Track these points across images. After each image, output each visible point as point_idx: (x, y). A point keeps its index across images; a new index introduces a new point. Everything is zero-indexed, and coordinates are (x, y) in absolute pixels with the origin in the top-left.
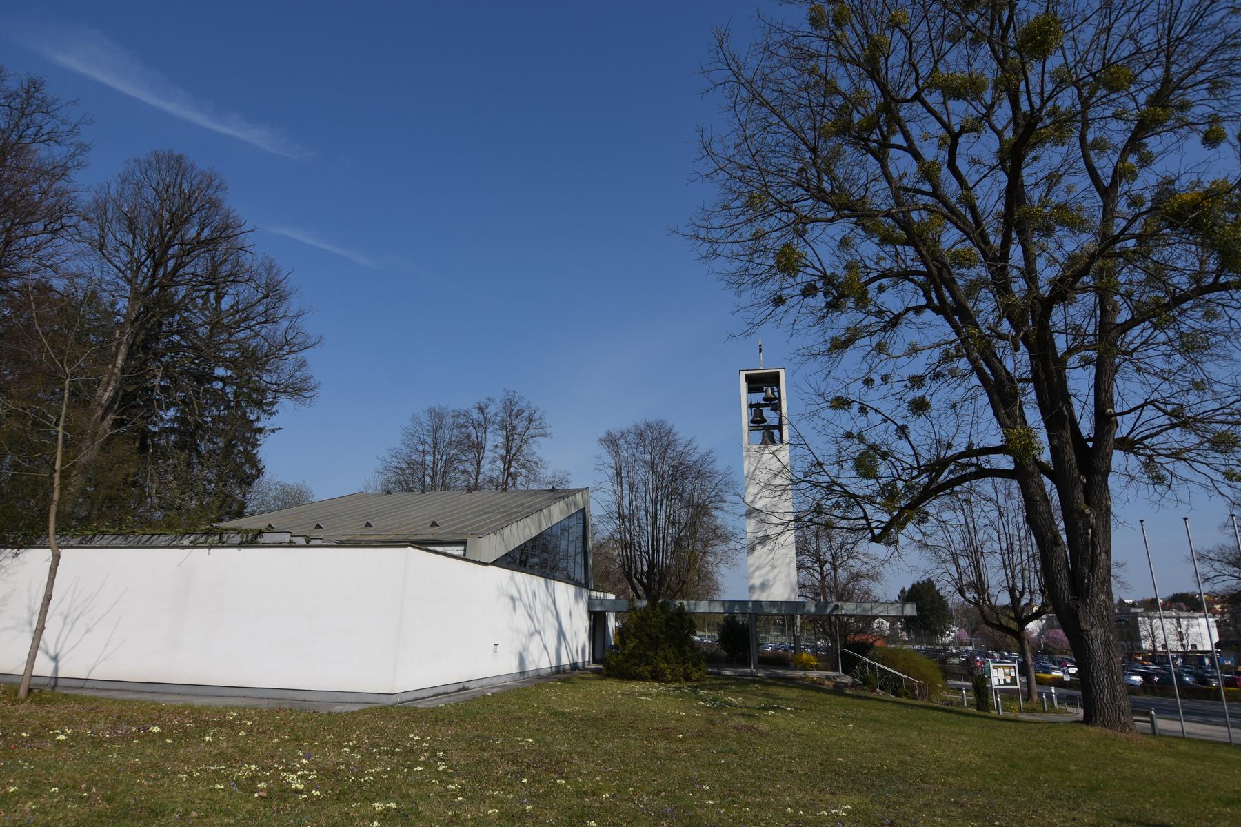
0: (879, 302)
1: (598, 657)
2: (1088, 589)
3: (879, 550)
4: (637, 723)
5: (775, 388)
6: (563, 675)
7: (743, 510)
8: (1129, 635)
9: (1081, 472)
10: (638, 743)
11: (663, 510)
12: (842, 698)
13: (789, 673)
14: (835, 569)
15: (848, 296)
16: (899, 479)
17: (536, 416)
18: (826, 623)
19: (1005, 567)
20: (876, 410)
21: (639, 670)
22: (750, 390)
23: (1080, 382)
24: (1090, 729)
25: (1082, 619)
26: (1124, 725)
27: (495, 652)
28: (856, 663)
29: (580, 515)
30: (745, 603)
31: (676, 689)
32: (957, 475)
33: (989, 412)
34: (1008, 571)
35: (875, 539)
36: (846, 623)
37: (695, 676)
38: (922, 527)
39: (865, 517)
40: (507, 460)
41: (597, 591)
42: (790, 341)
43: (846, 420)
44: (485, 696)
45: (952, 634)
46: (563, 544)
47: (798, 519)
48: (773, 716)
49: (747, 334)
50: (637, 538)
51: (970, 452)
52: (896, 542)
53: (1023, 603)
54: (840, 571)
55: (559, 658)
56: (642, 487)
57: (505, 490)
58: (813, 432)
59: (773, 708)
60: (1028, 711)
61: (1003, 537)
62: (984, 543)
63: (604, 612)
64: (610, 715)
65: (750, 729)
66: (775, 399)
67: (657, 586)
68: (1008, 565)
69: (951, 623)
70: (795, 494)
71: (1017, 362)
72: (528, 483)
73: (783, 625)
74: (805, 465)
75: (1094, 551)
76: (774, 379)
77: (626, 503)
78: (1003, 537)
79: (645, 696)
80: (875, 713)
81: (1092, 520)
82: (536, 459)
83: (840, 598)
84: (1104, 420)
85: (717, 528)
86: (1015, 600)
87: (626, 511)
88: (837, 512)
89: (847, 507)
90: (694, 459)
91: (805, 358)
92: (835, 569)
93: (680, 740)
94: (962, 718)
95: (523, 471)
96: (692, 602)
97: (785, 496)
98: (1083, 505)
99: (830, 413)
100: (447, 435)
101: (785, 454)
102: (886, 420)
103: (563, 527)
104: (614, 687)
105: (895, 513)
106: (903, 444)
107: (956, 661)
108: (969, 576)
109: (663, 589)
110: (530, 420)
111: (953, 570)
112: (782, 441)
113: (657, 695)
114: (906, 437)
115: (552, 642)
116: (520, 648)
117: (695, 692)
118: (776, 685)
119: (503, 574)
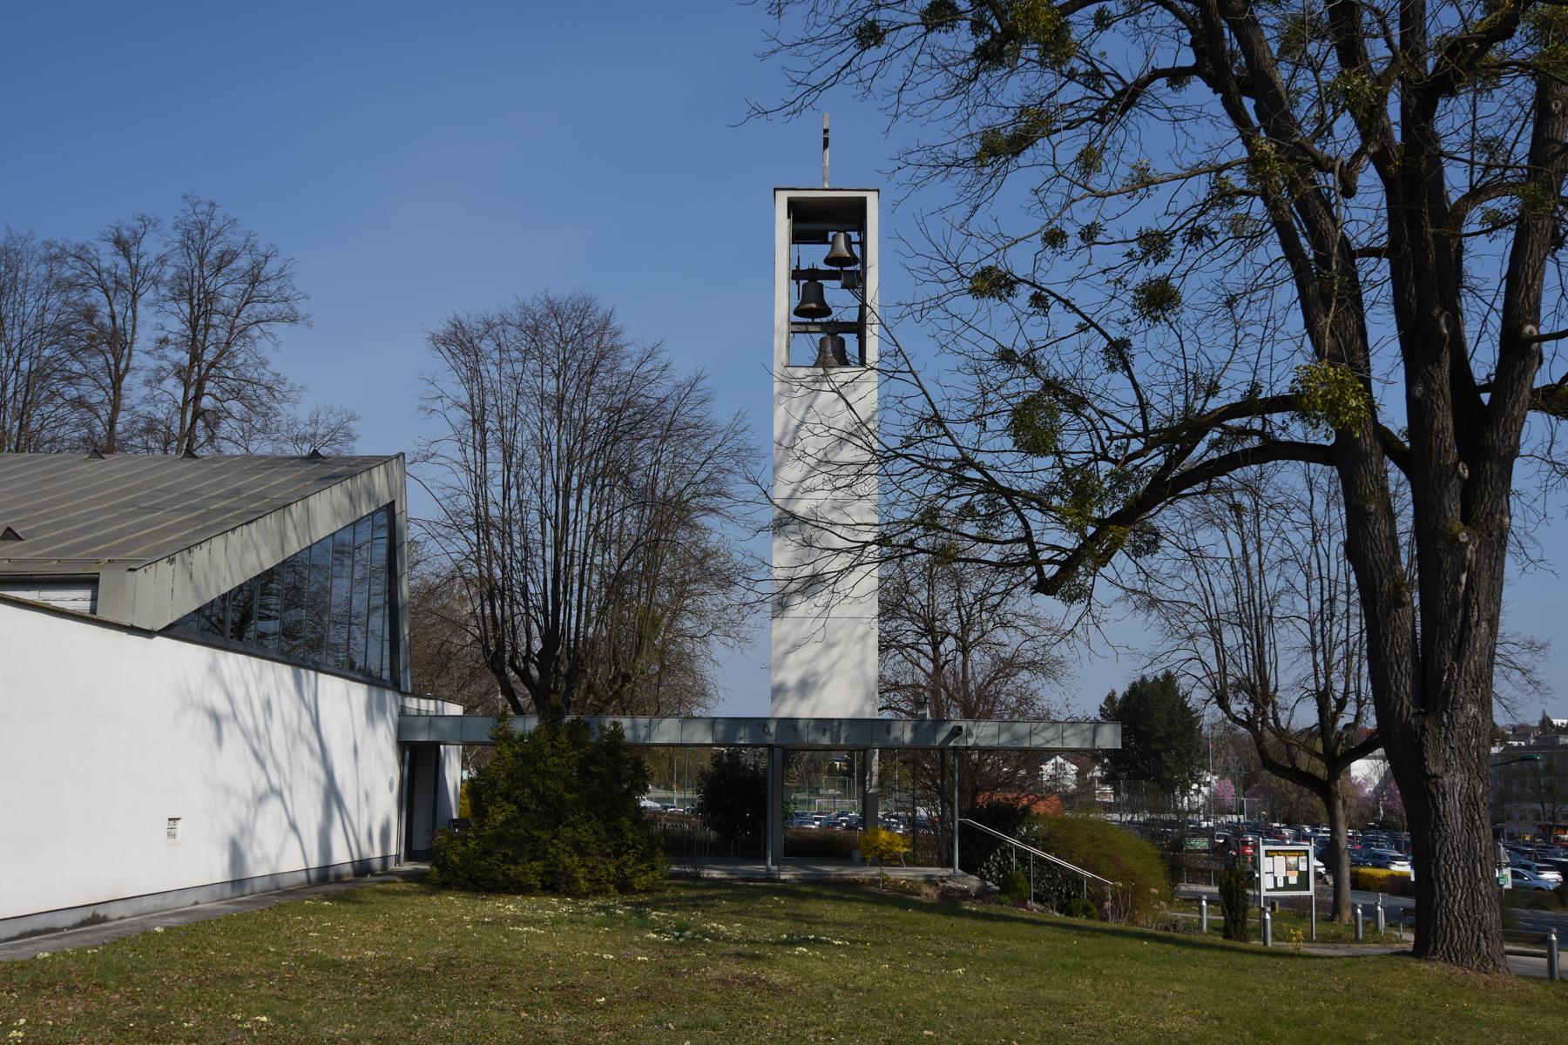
0: (1094, 52)
1: (419, 845)
2: (1447, 693)
3: (1049, 607)
4: (507, 979)
5: (855, 236)
6: (331, 886)
7: (768, 516)
8: (1550, 789)
9: (1462, 457)
10: (508, 1017)
11: (583, 511)
12: (953, 920)
13: (850, 872)
14: (965, 649)
15: (1023, 39)
16: (1105, 458)
17: (271, 268)
18: (938, 767)
19: (1314, 650)
20: (1067, 303)
21: (514, 870)
22: (798, 237)
23: (1486, 260)
24: (1423, 966)
25: (1429, 755)
26: (1485, 959)
27: (171, 835)
28: (991, 849)
29: (382, 519)
30: (760, 723)
31: (599, 908)
32: (1225, 452)
33: (1296, 320)
34: (1320, 657)
35: (1045, 587)
36: (978, 766)
37: (642, 881)
38: (1146, 561)
39: (1028, 538)
40: (194, 378)
41: (420, 696)
42: (892, 131)
43: (1003, 322)
44: (148, 935)
45: (1206, 788)
46: (340, 588)
47: (883, 541)
48: (803, 956)
49: (793, 109)
50: (518, 576)
51: (1252, 404)
52: (1085, 594)
53: (1341, 723)
54: (976, 655)
55: (326, 849)
56: (533, 455)
57: (190, 454)
58: (931, 349)
59: (805, 942)
60: (1325, 939)
61: (1316, 585)
62: (1276, 597)
63: (436, 745)
64: (447, 965)
65: (752, 983)
66: (854, 260)
67: (562, 687)
68: (1319, 645)
69: (1203, 767)
70: (881, 485)
71: (1365, 213)
72: (247, 436)
73: (849, 774)
74: (908, 420)
75: (1466, 617)
76: (851, 214)
77: (495, 492)
78: (1316, 585)
79: (528, 924)
80: (1014, 945)
81: (1470, 553)
82: (267, 378)
83: (969, 713)
84: (1518, 348)
85: (707, 554)
86: (1327, 719)
87: (494, 511)
88: (970, 528)
89: (990, 517)
90: (660, 393)
91: (923, 172)
92: (965, 649)
93: (601, 1007)
94: (1187, 951)
95: (235, 406)
96: (643, 721)
97: (860, 489)
98: (1457, 525)
99: (966, 304)
100: (31, 308)
101: (867, 393)
102: (1087, 325)
103: (339, 548)
104: (456, 907)
105: (1091, 530)
106: (1119, 379)
107: (1201, 843)
108: (1240, 669)
109: (577, 694)
110: (254, 278)
111: (1209, 654)
112: (863, 363)
113: (555, 922)
114: (1126, 367)
115: (309, 814)
116: (232, 829)
117: (640, 915)
118: (818, 896)
119: (193, 656)
